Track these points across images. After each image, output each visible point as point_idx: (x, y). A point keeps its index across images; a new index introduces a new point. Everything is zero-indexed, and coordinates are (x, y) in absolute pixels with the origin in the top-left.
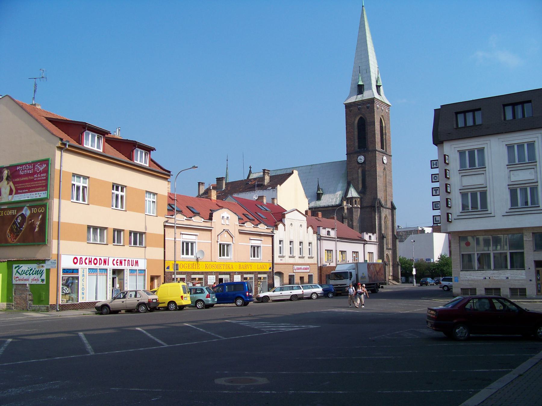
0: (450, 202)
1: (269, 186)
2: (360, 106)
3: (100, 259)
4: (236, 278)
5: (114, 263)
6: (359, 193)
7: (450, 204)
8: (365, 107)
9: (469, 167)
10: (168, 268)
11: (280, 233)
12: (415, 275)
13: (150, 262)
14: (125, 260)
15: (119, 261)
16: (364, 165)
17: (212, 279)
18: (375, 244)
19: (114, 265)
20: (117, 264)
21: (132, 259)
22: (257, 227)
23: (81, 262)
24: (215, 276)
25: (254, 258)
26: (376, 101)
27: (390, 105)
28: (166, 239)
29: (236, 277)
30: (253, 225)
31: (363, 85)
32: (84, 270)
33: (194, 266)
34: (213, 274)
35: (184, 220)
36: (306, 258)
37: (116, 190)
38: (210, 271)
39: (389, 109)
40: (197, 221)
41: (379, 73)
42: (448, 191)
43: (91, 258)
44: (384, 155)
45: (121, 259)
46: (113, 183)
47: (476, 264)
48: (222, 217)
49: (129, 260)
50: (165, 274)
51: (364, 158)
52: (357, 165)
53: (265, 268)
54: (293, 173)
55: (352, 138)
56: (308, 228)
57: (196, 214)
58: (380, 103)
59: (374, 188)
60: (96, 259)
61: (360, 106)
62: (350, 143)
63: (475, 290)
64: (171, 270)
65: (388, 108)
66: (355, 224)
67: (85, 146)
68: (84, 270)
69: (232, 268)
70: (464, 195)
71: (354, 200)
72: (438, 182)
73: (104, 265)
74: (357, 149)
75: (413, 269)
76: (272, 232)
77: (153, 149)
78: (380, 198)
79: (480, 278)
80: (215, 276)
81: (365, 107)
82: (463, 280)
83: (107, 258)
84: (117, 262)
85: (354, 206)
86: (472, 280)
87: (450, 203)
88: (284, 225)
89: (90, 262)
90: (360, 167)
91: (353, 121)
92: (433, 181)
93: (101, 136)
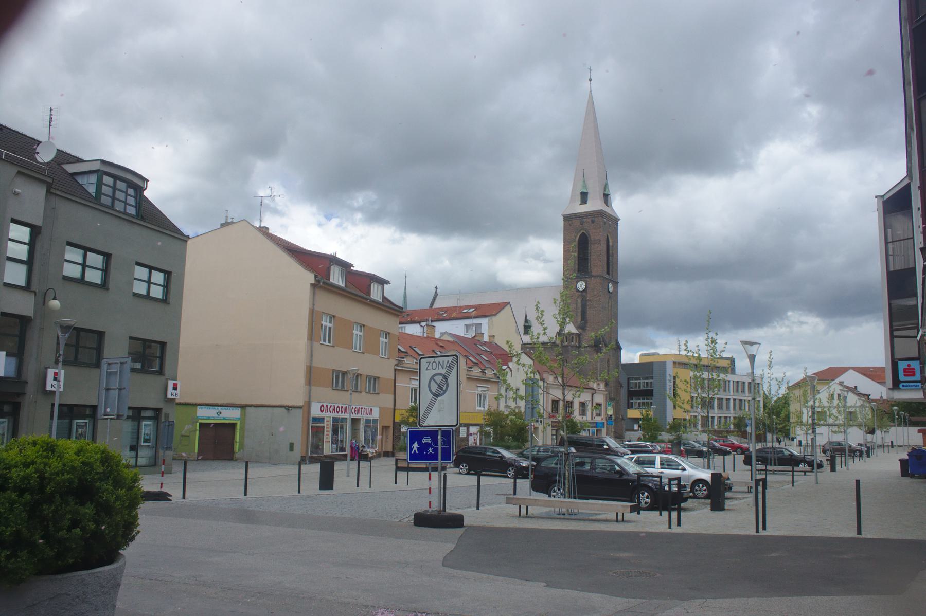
3: (342, 407)
6: (578, 328)
8: (589, 220)
13: (382, 410)
14: (362, 408)
15: (356, 409)
16: (584, 294)
19: (353, 413)
22: (470, 370)
28: (397, 384)
44: (609, 281)
49: (365, 408)
50: (394, 425)
60: (338, 407)
67: (371, 297)
84: (355, 411)
89: (334, 410)
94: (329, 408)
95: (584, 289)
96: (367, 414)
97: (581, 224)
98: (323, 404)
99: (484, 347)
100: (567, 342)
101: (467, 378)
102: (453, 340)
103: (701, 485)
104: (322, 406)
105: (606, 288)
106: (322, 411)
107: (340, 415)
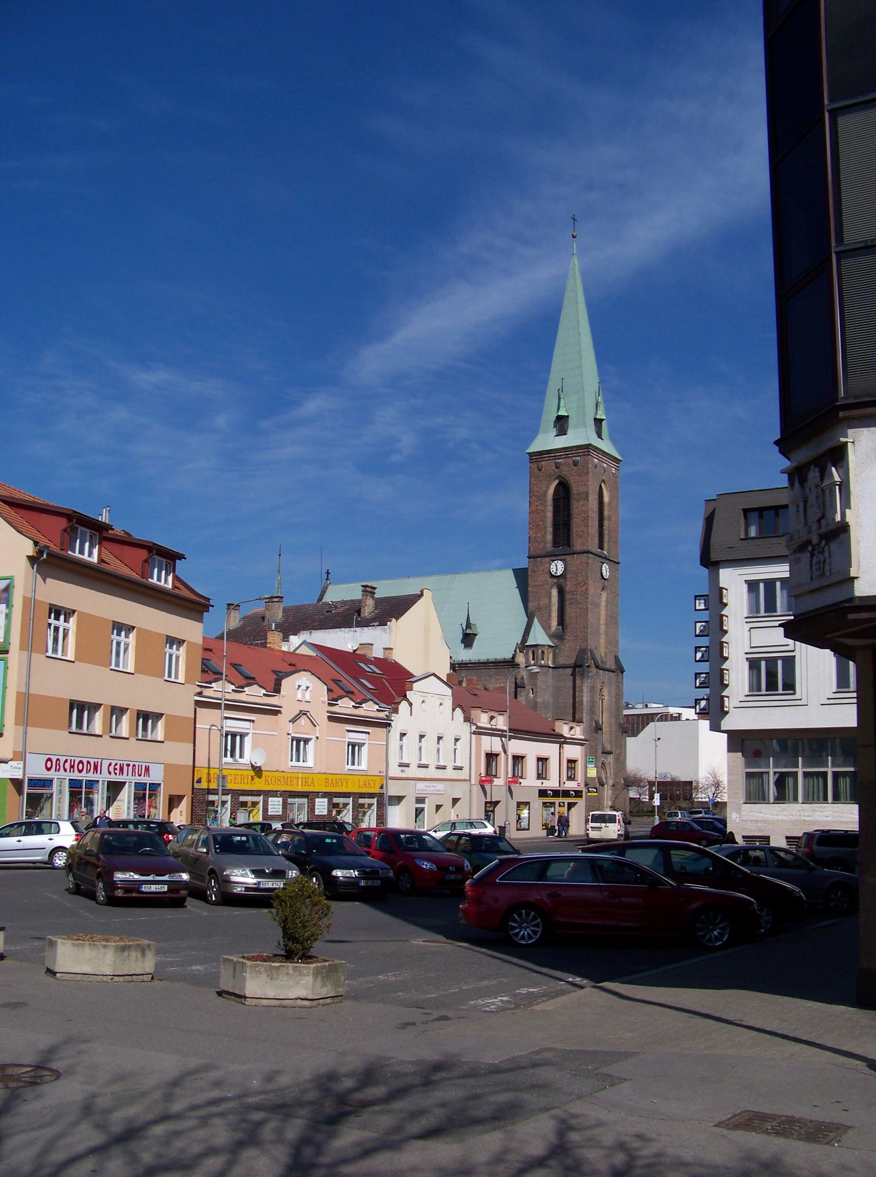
0: (727, 676)
1: (374, 620)
2: (559, 460)
3: (88, 762)
4: (319, 804)
5: (110, 770)
6: (552, 636)
7: (727, 678)
8: (570, 461)
9: (765, 613)
10: (199, 781)
11: (402, 719)
12: (658, 806)
14: (128, 765)
15: (118, 767)
16: (562, 581)
17: (275, 805)
18: (582, 745)
19: (110, 773)
20: (116, 771)
21: (140, 764)
23: (58, 767)
24: (281, 799)
25: (298, 764)
26: (593, 452)
27: (620, 458)
28: (197, 726)
29: (272, 801)
30: (353, 704)
31: (568, 416)
32: (61, 782)
33: (246, 780)
34: (278, 795)
35: (231, 691)
36: (432, 768)
37: (55, 619)
38: (273, 790)
39: (618, 467)
40: (254, 694)
41: (601, 394)
42: (725, 655)
43: (74, 760)
44: (603, 561)
45: (122, 762)
46: (50, 604)
47: (772, 791)
48: (297, 687)
51: (563, 566)
52: (549, 579)
53: (372, 786)
54: (422, 595)
55: (541, 523)
56: (454, 710)
57: (250, 680)
58: (600, 456)
59: (581, 629)
60: (81, 762)
61: (559, 459)
62: (537, 534)
63: (767, 839)
64: (204, 785)
65: (617, 465)
66: (540, 699)
68: (61, 782)
69: (312, 785)
70: (754, 664)
71: (540, 651)
72: (707, 636)
73: (94, 773)
74: (549, 546)
75: (655, 794)
76: (388, 718)
77: (181, 557)
78: (593, 648)
79: (778, 818)
80: (281, 799)
81: (570, 461)
82: (746, 820)
83: (100, 761)
84: (115, 769)
85: (539, 662)
86: (764, 821)
87: (726, 677)
88: (411, 704)
89: (72, 767)
90: (555, 583)
91: (544, 489)
92: (697, 624)
93: (95, 533)
94: (62, 764)
95: (559, 574)
96: (140, 775)
97: (558, 468)
98: (81, 759)
99: (368, 670)
100: (533, 659)
101: (329, 717)
102: (315, 655)
103: (832, 896)
104: (49, 760)
105: (599, 572)
106: (49, 769)
107: (84, 776)
